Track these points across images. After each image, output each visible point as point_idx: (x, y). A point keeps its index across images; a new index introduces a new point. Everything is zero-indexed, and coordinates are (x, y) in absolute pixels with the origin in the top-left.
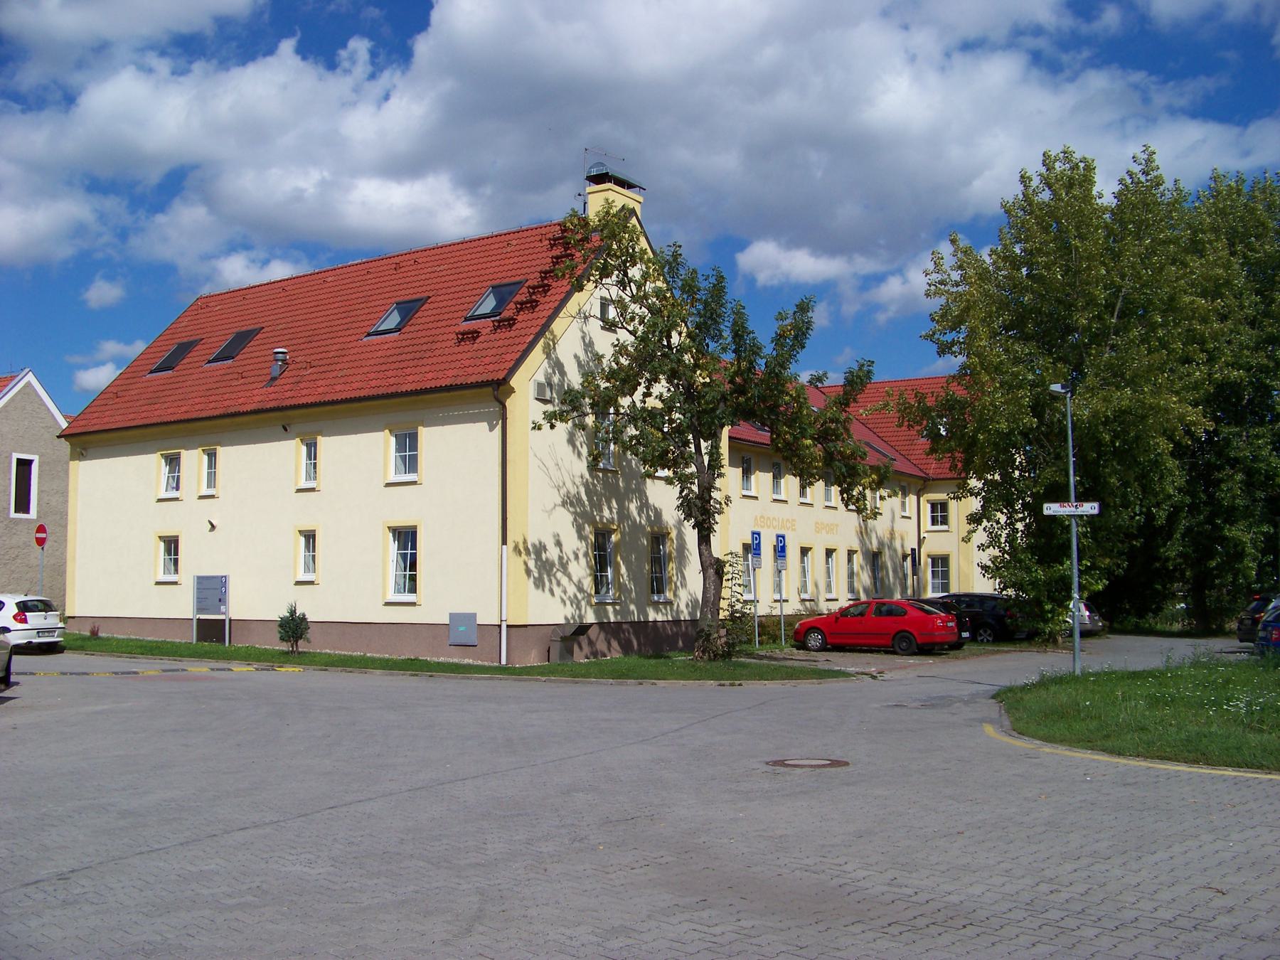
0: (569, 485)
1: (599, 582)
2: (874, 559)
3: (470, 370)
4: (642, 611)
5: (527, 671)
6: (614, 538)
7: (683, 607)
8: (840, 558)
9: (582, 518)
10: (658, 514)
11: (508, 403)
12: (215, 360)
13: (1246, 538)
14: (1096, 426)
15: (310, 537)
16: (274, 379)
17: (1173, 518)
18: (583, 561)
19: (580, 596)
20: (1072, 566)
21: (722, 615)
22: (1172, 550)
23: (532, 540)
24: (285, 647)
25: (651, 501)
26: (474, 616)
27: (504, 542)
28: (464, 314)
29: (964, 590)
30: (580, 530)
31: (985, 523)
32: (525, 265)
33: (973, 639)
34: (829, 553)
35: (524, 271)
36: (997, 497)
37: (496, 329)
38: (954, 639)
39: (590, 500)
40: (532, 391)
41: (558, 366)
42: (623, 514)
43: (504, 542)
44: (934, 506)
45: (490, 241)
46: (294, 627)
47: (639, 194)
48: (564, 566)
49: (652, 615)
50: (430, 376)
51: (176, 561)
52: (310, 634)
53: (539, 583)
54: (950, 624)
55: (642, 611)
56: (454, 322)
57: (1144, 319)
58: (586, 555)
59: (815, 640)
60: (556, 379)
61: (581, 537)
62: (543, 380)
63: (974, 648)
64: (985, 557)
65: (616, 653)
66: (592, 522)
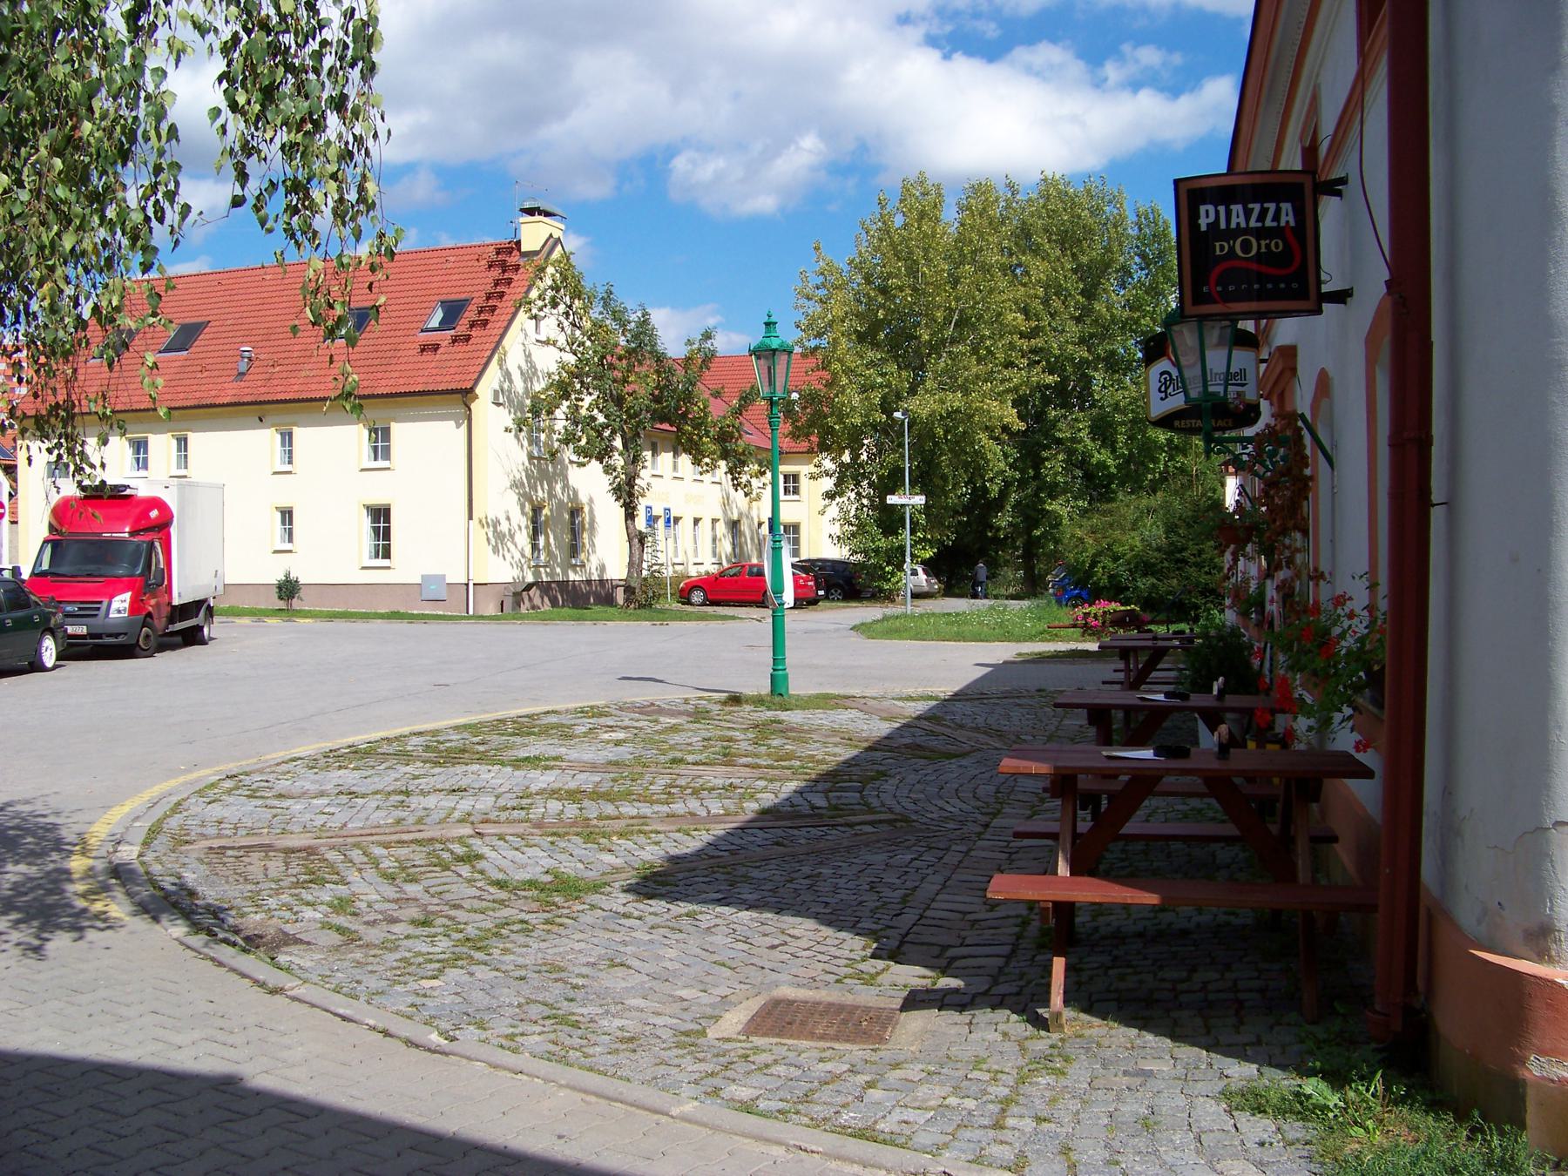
0: (515, 471)
1: (535, 547)
2: (734, 526)
3: (439, 379)
4: (565, 573)
5: (491, 618)
6: (546, 511)
7: (593, 570)
8: (705, 525)
9: (525, 497)
10: (576, 493)
11: (473, 406)
12: (166, 350)
13: (1064, 512)
14: (933, 424)
15: (287, 515)
16: (243, 374)
17: (1004, 494)
18: (524, 532)
19: (523, 561)
20: (906, 536)
21: (645, 573)
22: (1003, 520)
23: (491, 516)
24: (282, 605)
25: (571, 482)
26: (444, 577)
27: (470, 517)
28: (420, 325)
29: (814, 556)
30: (522, 507)
31: (838, 499)
32: (468, 282)
33: (826, 598)
34: (696, 521)
35: (470, 288)
36: (847, 476)
37: (454, 341)
38: (812, 595)
39: (529, 483)
40: (490, 397)
41: (507, 375)
42: (551, 495)
43: (470, 517)
44: (786, 477)
45: (428, 255)
46: (288, 589)
47: (561, 222)
48: (512, 536)
49: (572, 576)
50: (401, 381)
51: (290, 531)
52: (302, 593)
53: (496, 550)
54: (810, 583)
55: (565, 573)
56: (412, 332)
57: (974, 328)
58: (527, 527)
59: (697, 597)
60: (506, 386)
61: (523, 513)
62: (498, 388)
63: (828, 604)
64: (836, 530)
65: (547, 606)
66: (531, 501)
